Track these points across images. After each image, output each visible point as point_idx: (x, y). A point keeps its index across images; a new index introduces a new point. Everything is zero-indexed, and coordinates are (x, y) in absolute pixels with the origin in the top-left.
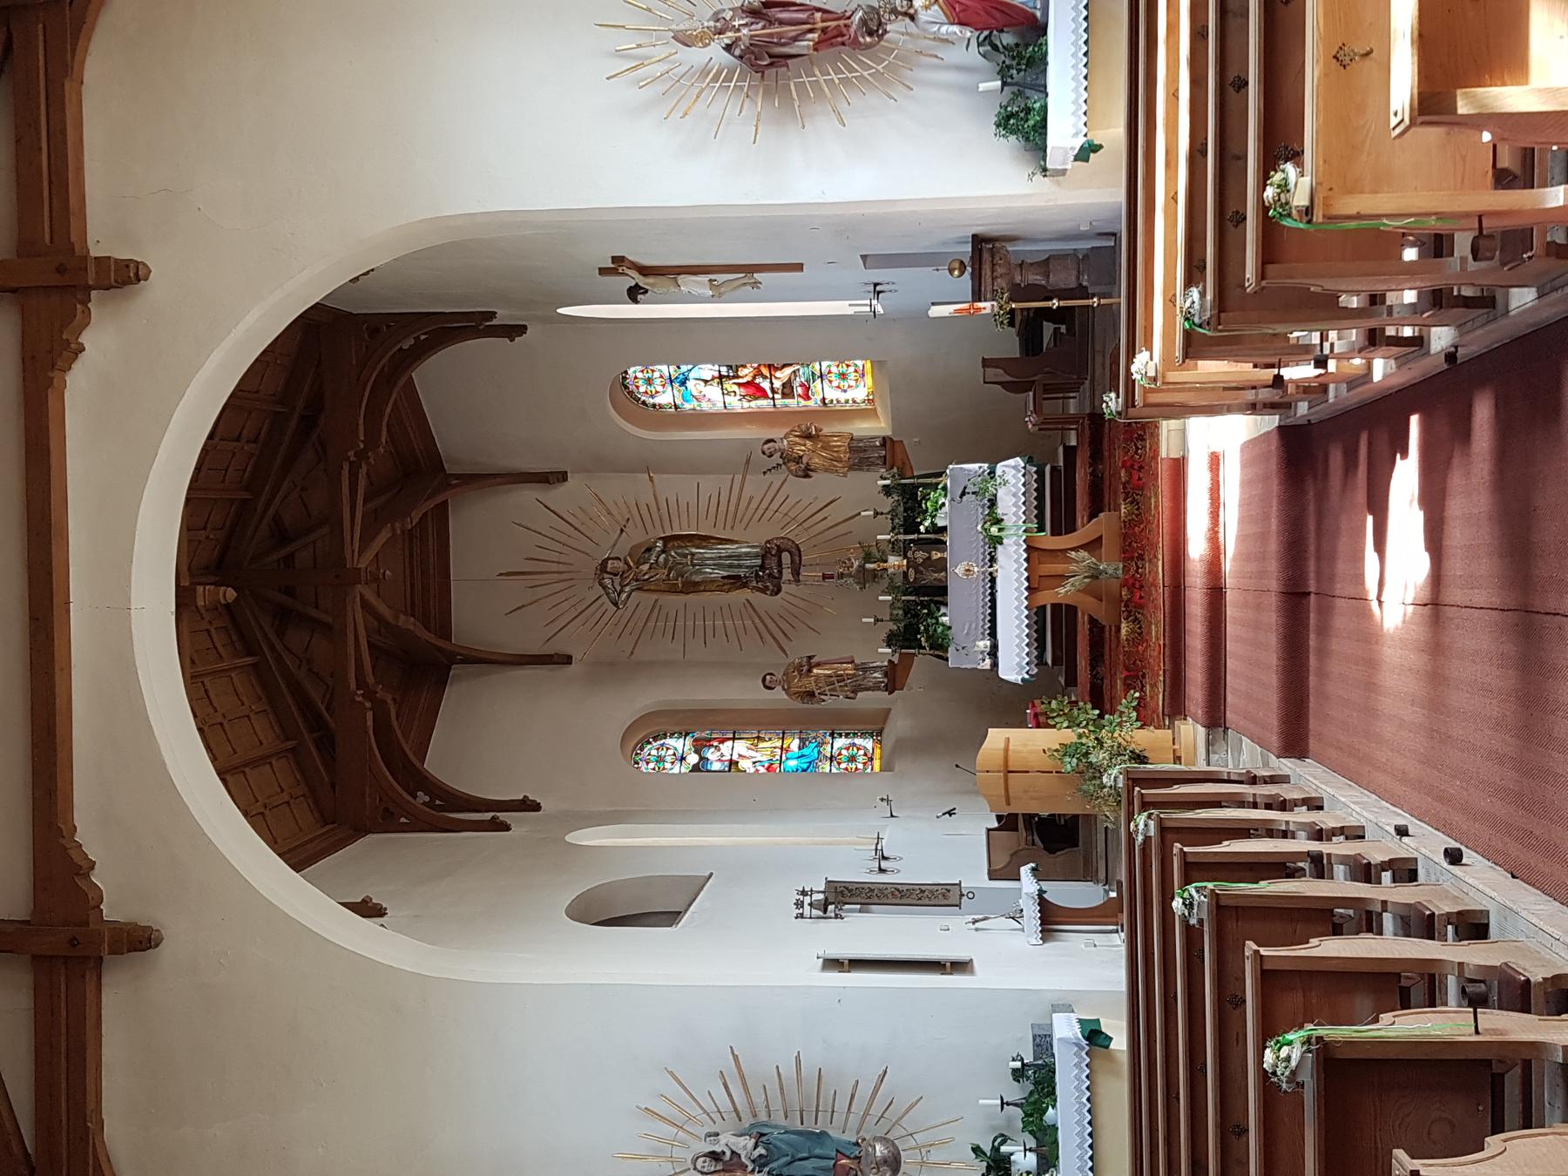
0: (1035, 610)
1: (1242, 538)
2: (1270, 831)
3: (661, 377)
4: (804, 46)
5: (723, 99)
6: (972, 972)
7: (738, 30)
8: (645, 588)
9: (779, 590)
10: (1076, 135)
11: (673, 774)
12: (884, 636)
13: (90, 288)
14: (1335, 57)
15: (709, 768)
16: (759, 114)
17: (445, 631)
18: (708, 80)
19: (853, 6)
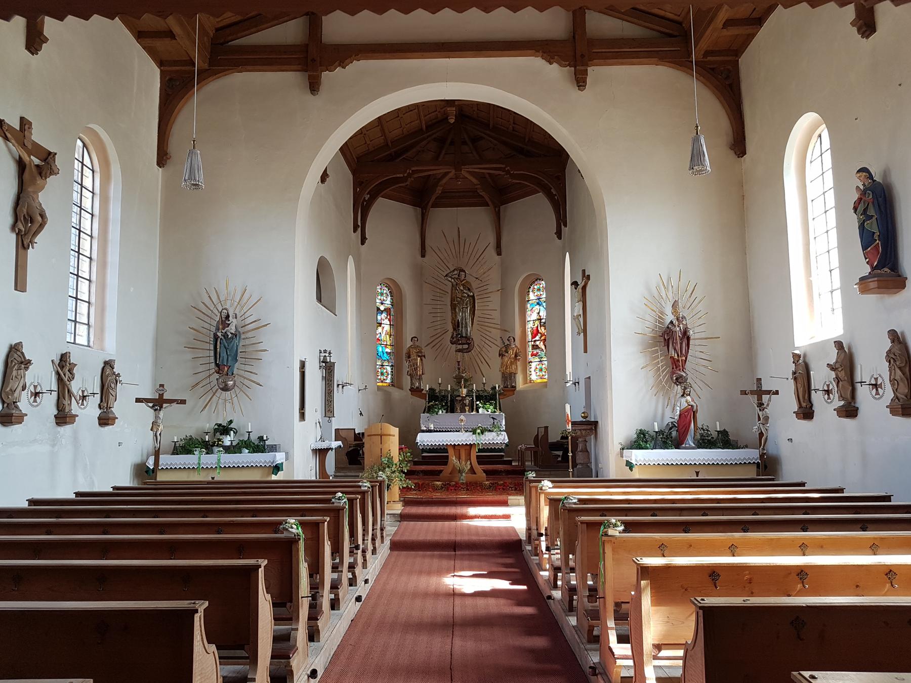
0: (446, 448)
1: (476, 527)
2: (365, 531)
3: (541, 295)
5: (652, 320)
6: (300, 421)
7: (678, 326)
9: (452, 344)
10: (636, 461)
11: (376, 300)
12: (434, 387)
13: (575, 67)
14: (663, 544)
15: (379, 315)
16: (646, 335)
17: (435, 205)
19: (688, 372)
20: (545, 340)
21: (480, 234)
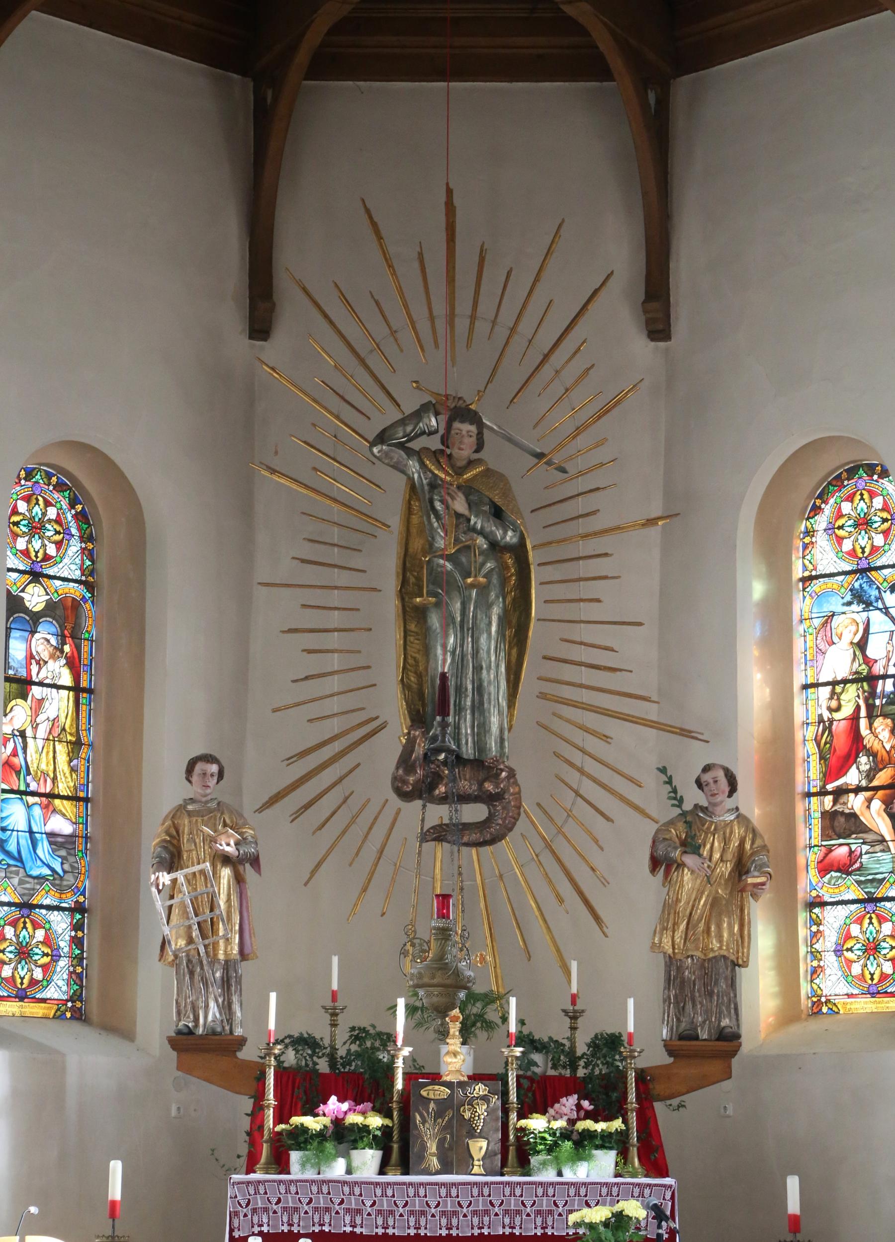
8: (415, 505)
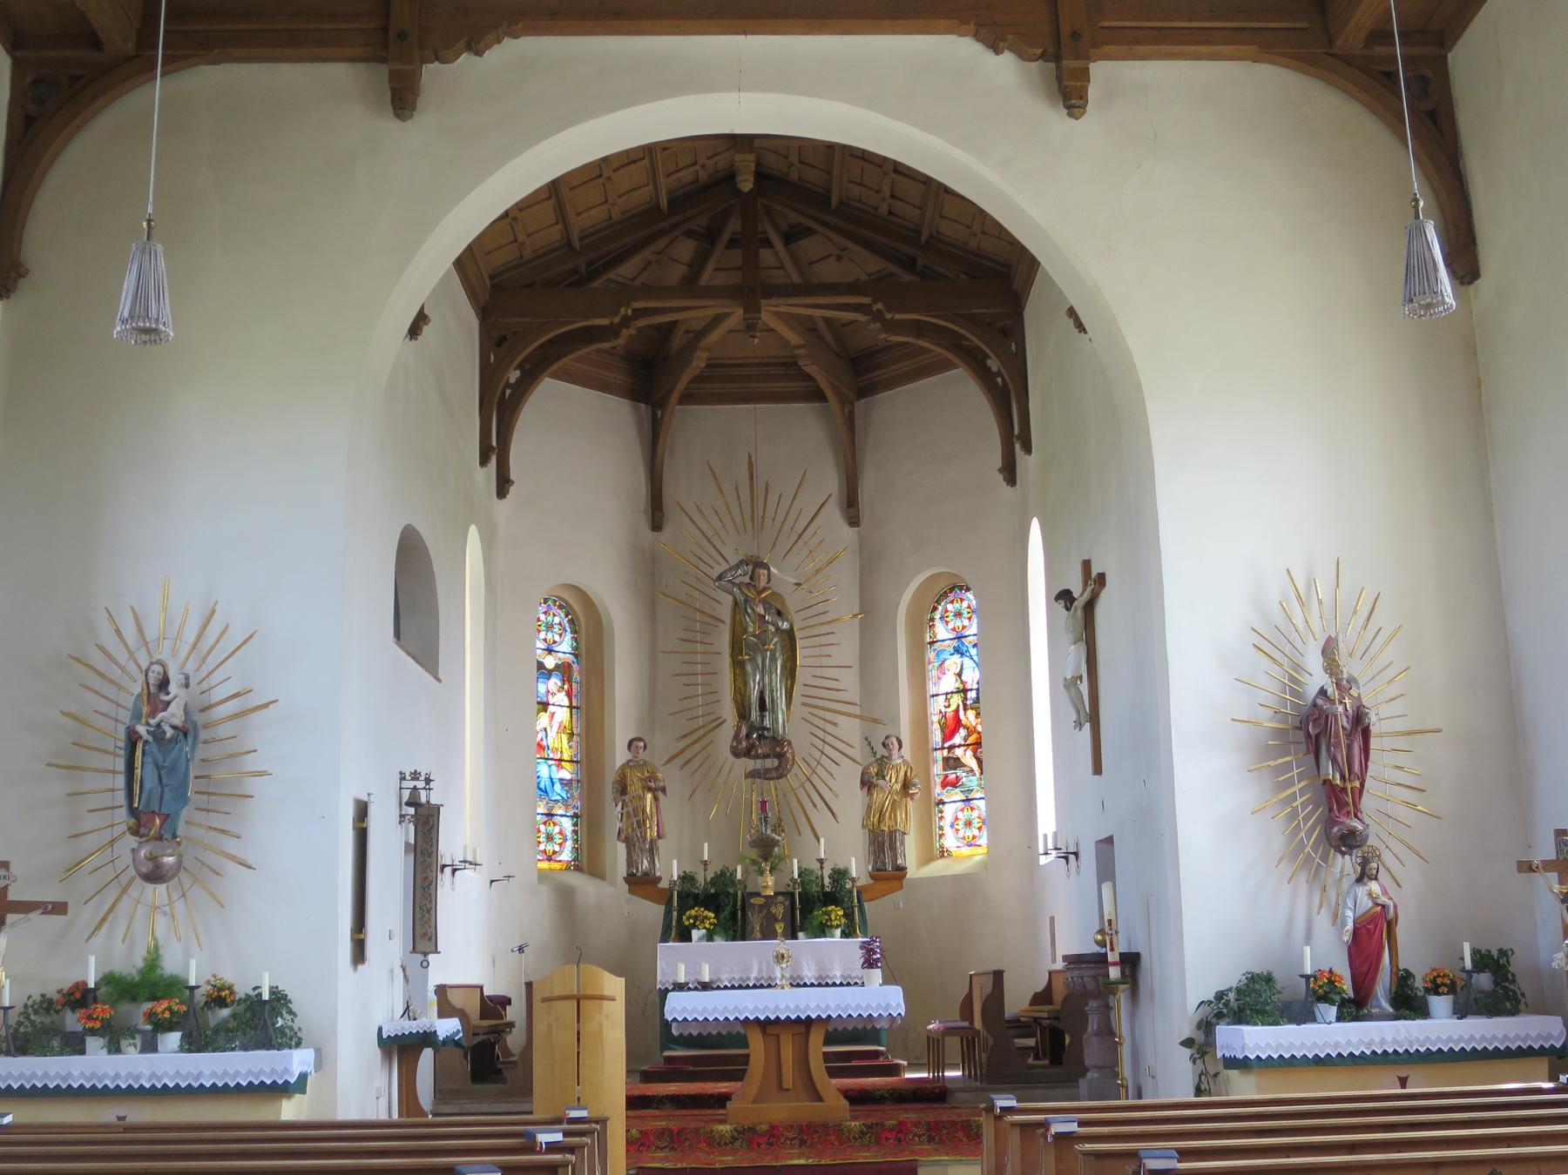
4: (1328, 770)
5: (1274, 687)
7: (1341, 702)
8: (737, 610)
15: (541, 680)
17: (688, 398)
18: (1292, 672)
19: (1367, 820)
20: (978, 744)
21: (806, 470)
